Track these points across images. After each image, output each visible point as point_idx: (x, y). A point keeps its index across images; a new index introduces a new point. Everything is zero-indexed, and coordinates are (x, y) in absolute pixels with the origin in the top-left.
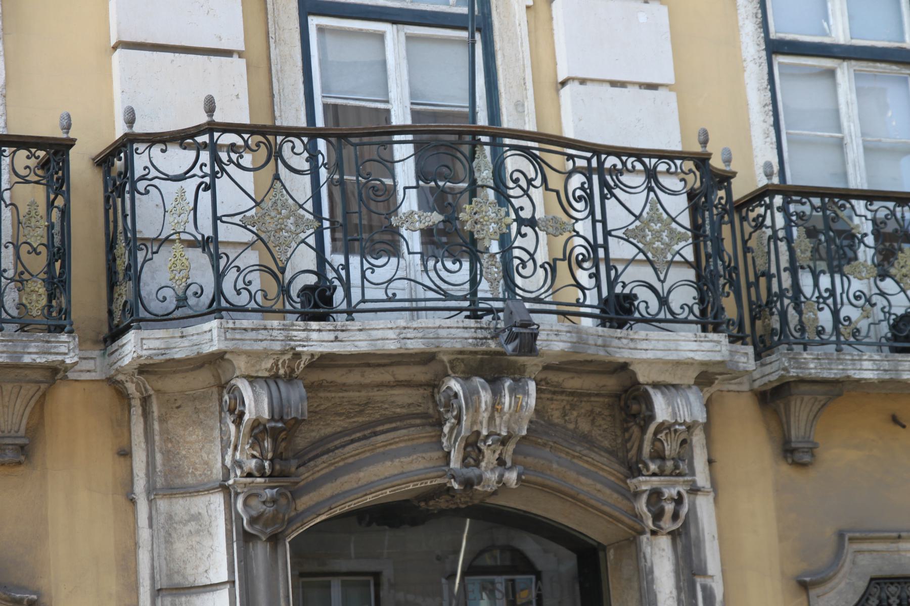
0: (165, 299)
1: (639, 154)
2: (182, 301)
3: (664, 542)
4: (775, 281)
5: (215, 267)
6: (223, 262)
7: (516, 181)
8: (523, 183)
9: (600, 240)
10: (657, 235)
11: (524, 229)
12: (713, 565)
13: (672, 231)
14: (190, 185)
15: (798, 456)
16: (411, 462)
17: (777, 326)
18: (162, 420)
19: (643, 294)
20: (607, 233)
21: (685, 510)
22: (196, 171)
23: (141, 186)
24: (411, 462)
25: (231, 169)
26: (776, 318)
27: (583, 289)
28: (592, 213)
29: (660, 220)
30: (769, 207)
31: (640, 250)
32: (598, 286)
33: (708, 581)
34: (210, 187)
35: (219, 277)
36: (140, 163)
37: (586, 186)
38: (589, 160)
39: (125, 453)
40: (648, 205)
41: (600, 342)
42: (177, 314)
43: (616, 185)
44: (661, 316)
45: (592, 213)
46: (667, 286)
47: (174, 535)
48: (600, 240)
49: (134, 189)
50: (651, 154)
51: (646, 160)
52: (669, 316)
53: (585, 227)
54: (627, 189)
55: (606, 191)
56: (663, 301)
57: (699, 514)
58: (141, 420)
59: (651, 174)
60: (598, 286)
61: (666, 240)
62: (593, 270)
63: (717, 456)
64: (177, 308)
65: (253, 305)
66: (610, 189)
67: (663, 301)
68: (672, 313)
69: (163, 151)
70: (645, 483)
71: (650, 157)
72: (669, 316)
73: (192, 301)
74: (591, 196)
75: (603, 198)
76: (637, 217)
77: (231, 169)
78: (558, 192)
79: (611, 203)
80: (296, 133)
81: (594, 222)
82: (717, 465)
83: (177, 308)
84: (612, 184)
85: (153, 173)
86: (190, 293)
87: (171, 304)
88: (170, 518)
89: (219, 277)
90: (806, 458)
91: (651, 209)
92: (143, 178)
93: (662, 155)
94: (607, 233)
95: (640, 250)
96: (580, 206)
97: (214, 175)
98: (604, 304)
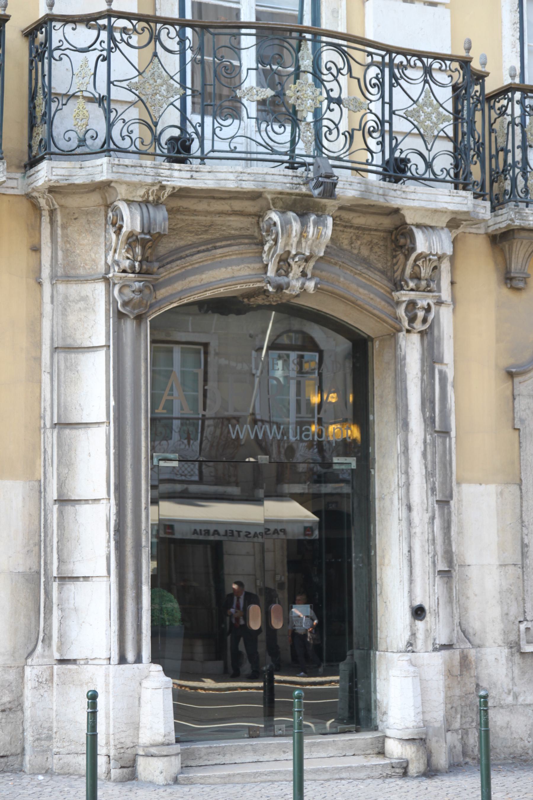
0: (70, 139)
1: (420, 55)
2: (82, 142)
3: (415, 338)
4: (510, 155)
5: (108, 119)
6: (113, 115)
7: (329, 69)
8: (334, 71)
9: (387, 118)
10: (428, 117)
11: (333, 106)
12: (448, 356)
13: (439, 114)
14: (92, 56)
15: (515, 283)
16: (240, 270)
17: (509, 188)
18: (64, 227)
19: (415, 159)
20: (392, 112)
21: (431, 317)
22: (97, 45)
23: (56, 54)
24: (240, 270)
25: (122, 46)
26: (508, 182)
27: (371, 152)
28: (382, 97)
29: (431, 105)
30: (511, 100)
31: (415, 126)
32: (383, 151)
33: (444, 368)
34: (107, 59)
35: (110, 126)
36: (56, 36)
37: (380, 76)
38: (383, 57)
39: (36, 249)
40: (424, 93)
41: (381, 192)
42: (78, 151)
43: (401, 77)
44: (427, 176)
45: (382, 97)
46: (432, 154)
47: (68, 310)
48: (387, 118)
49: (51, 56)
50: (429, 55)
51: (425, 60)
52: (432, 177)
53: (376, 107)
54: (409, 80)
55: (394, 81)
56: (429, 165)
57: (441, 320)
58: (49, 226)
59: (428, 71)
60: (383, 151)
61: (435, 120)
62: (380, 139)
63: (458, 279)
64: (79, 146)
65: (133, 148)
66: (397, 79)
67: (429, 165)
68: (434, 174)
69: (74, 29)
70: (405, 296)
71: (428, 57)
72: (432, 177)
73: (89, 142)
74: (382, 84)
75: (391, 86)
76: (415, 102)
77: (122, 46)
78: (359, 80)
79: (397, 90)
80: (171, 22)
81: (383, 103)
82: (457, 286)
83: (79, 146)
84: (398, 76)
85: (66, 45)
86: (88, 136)
87: (74, 143)
88: (66, 297)
89: (110, 126)
90: (521, 285)
91: (426, 97)
92: (58, 48)
93: (436, 57)
94: (392, 112)
95: (415, 126)
96: (374, 91)
97: (110, 50)
98: (386, 164)
